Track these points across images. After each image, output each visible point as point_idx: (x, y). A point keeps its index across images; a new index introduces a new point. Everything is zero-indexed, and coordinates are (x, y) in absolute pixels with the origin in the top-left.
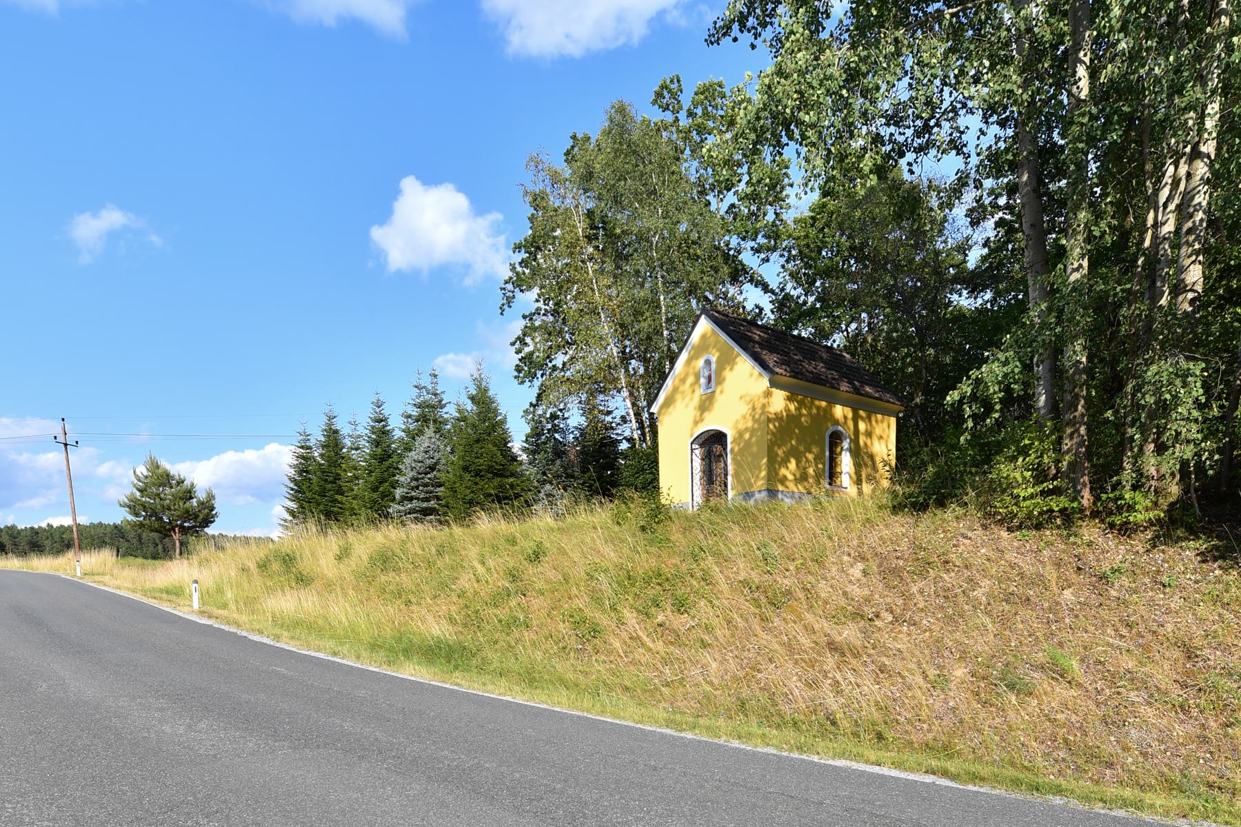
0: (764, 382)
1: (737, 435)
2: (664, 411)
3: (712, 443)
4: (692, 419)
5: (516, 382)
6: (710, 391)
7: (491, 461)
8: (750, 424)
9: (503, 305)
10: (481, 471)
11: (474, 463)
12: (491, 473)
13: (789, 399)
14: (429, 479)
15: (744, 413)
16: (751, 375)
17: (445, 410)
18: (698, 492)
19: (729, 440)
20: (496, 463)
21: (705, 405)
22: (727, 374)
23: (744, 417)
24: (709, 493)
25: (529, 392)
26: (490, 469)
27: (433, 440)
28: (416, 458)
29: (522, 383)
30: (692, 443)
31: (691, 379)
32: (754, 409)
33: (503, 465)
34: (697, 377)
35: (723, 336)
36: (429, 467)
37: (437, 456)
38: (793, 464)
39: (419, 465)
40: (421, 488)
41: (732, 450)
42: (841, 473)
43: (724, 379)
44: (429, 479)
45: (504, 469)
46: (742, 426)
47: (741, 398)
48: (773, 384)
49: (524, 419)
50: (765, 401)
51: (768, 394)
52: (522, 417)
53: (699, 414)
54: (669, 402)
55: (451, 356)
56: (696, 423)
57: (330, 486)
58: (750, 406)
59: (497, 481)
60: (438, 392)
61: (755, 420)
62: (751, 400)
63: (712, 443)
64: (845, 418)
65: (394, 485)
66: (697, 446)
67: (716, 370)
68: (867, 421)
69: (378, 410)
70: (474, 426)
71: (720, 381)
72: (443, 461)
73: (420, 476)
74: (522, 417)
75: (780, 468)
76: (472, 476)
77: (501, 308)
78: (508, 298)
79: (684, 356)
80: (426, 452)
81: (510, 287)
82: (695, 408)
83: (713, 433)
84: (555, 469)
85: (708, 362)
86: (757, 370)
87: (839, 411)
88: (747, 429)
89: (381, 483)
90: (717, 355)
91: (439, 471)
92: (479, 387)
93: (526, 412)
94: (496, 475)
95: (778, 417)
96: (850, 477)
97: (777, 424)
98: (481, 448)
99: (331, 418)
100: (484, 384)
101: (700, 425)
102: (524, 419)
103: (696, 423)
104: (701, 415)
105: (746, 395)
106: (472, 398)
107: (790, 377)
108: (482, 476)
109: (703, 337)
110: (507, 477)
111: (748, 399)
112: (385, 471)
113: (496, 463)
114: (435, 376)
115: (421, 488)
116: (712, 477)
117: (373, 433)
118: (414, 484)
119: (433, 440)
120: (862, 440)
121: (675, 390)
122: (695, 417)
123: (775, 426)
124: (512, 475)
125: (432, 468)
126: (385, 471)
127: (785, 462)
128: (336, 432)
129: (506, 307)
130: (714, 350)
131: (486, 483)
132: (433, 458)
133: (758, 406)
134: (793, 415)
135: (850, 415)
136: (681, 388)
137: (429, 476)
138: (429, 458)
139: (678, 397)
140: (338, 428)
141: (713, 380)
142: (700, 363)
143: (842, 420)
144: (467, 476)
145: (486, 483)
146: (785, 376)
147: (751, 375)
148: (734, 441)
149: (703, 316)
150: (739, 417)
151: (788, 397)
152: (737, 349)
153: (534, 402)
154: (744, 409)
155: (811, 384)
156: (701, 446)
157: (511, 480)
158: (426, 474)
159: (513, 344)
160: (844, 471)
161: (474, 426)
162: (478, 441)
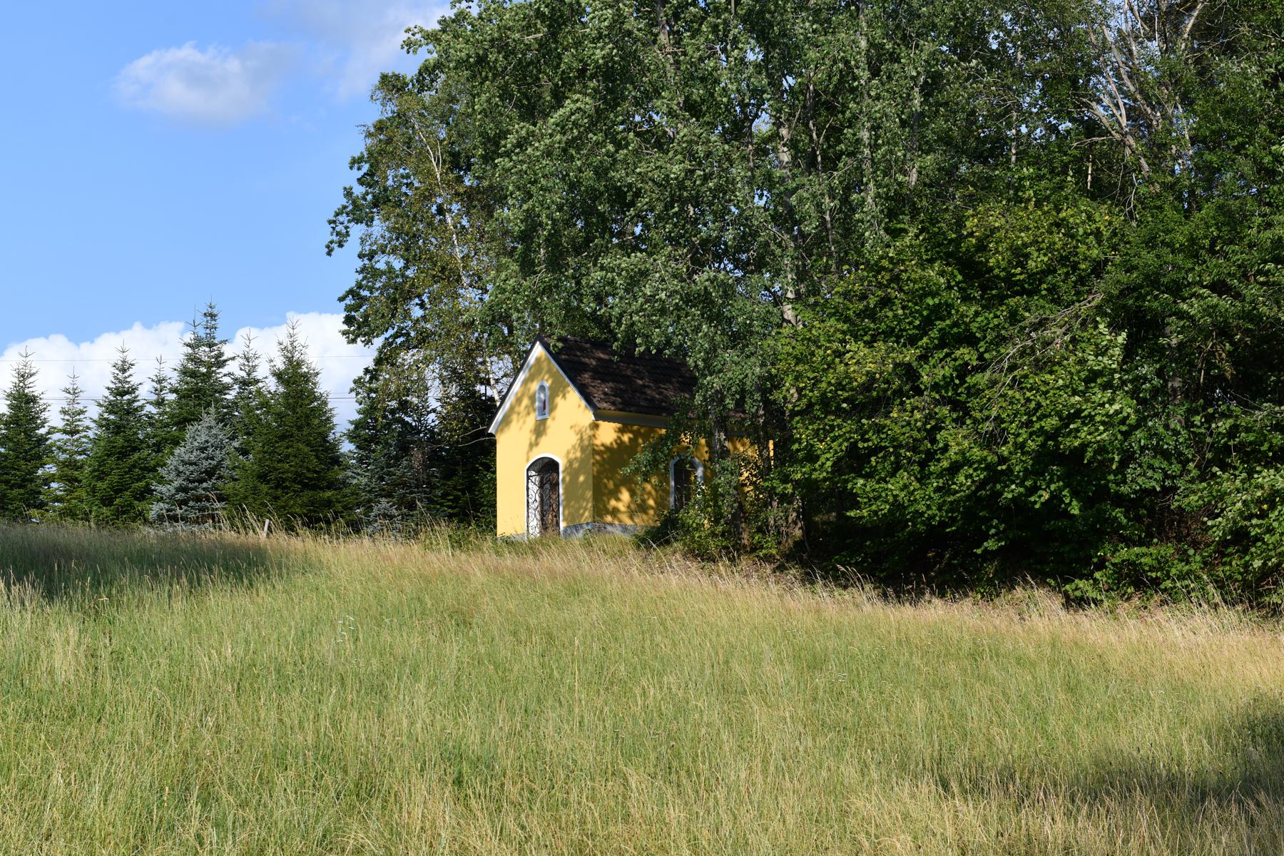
0: (589, 416)
3: (546, 469)
4: (527, 443)
5: (344, 339)
7: (301, 467)
8: (578, 454)
9: (332, 242)
10: (284, 480)
11: (276, 470)
12: (298, 483)
14: (204, 489)
17: (224, 370)
18: (535, 522)
19: (561, 468)
20: (309, 470)
21: (540, 430)
22: (559, 400)
23: (574, 447)
24: (544, 526)
25: (363, 356)
26: (298, 478)
27: (214, 431)
28: (186, 458)
29: (354, 341)
30: (528, 470)
32: (582, 439)
33: (316, 472)
35: (556, 367)
36: (206, 472)
37: (218, 454)
38: (625, 496)
39: (191, 468)
40: (191, 503)
41: (564, 479)
44: (204, 489)
45: (318, 479)
46: (572, 456)
49: (353, 394)
51: (595, 426)
52: (352, 390)
54: (506, 421)
55: (186, 53)
56: (533, 445)
57: (15, 492)
58: (579, 436)
59: (307, 495)
60: (216, 341)
63: (546, 469)
65: (145, 494)
66: (534, 473)
69: (121, 376)
70: (280, 416)
71: (553, 409)
72: (227, 462)
73: (190, 485)
74: (352, 390)
75: (609, 500)
76: (271, 488)
77: (328, 247)
78: (338, 234)
80: (203, 449)
81: (343, 218)
83: (547, 461)
84: (398, 473)
86: (583, 403)
88: (576, 458)
89: (117, 492)
90: (550, 382)
91: (220, 477)
92: (290, 360)
93: (358, 382)
94: (306, 486)
95: (608, 449)
98: (287, 448)
99: (23, 377)
100: (297, 355)
101: (535, 449)
102: (353, 394)
103: (533, 445)
104: (536, 439)
106: (279, 376)
108: (287, 487)
109: (538, 360)
110: (322, 489)
111: (577, 429)
112: (126, 473)
113: (309, 470)
114: (213, 316)
115: (191, 503)
116: (548, 509)
117: (110, 413)
118: (180, 496)
119: (214, 431)
121: (512, 409)
124: (331, 485)
125: (210, 473)
126: (126, 473)
127: (615, 494)
128: (32, 400)
129: (335, 246)
131: (291, 498)
132: (212, 459)
133: (585, 437)
134: (626, 446)
136: (517, 409)
137: (205, 485)
138: (207, 459)
139: (514, 417)
140: (36, 394)
141: (546, 408)
144: (264, 488)
145: (291, 498)
150: (570, 447)
153: (372, 366)
154: (573, 439)
156: (539, 472)
157: (328, 494)
158: (201, 481)
159: (341, 299)
161: (280, 416)
162: (283, 437)
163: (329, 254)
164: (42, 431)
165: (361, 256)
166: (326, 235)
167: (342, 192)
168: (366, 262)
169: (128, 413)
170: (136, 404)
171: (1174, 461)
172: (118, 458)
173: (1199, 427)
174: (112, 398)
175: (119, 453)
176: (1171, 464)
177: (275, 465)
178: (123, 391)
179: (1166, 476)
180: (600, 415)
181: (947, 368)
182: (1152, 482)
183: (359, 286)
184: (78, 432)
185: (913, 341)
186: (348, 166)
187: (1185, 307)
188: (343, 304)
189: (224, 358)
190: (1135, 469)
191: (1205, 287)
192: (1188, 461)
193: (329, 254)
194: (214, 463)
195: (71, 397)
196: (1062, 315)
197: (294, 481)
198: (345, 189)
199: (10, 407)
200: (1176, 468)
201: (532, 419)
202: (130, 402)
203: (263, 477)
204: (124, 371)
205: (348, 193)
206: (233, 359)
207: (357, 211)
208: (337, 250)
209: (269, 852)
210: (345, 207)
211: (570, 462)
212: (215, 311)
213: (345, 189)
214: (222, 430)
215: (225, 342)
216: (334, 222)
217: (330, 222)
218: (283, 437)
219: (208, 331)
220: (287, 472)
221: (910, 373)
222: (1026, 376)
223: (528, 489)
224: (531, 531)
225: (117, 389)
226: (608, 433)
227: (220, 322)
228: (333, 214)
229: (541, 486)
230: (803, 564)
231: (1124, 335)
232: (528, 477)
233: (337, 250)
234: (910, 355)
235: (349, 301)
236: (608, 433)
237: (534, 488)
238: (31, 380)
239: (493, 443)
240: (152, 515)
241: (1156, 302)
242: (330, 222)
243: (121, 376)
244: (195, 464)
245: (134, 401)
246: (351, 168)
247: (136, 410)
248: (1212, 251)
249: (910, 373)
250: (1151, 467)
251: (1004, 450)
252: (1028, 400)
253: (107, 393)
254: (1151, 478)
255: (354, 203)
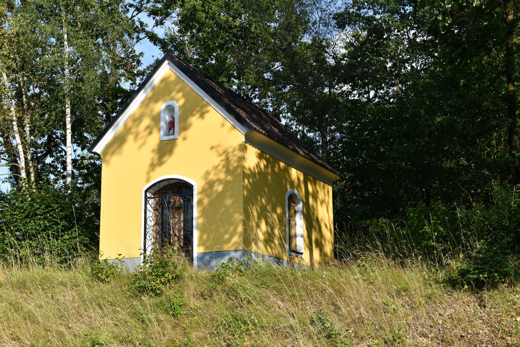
1: (207, 186)
2: (112, 149)
4: (149, 162)
6: (171, 137)
13: (260, 157)
15: (216, 164)
16: (223, 125)
22: (195, 120)
23: (216, 168)
31: (146, 122)
32: (227, 159)
34: (156, 119)
42: (296, 236)
43: (190, 125)
47: (212, 148)
48: (249, 140)
50: (240, 154)
51: (243, 148)
53: (156, 157)
56: (153, 166)
58: (223, 157)
61: (228, 171)
62: (225, 151)
64: (299, 179)
67: (180, 117)
68: (313, 184)
71: (185, 128)
79: (141, 97)
82: (153, 151)
85: (170, 109)
87: (294, 173)
95: (253, 174)
96: (304, 240)
97: (251, 181)
101: (158, 170)
103: (153, 166)
105: (218, 146)
107: (264, 134)
109: (164, 80)
111: (221, 150)
120: (311, 200)
121: (127, 131)
122: (153, 159)
123: (249, 181)
130: (180, 95)
135: (302, 178)
139: (130, 138)
142: (160, 106)
143: (296, 182)
146: (261, 133)
147: (223, 125)
148: (203, 191)
149: (166, 62)
150: (209, 167)
151: (259, 154)
152: (207, 98)
154: (217, 160)
155: (279, 144)
160: (298, 233)
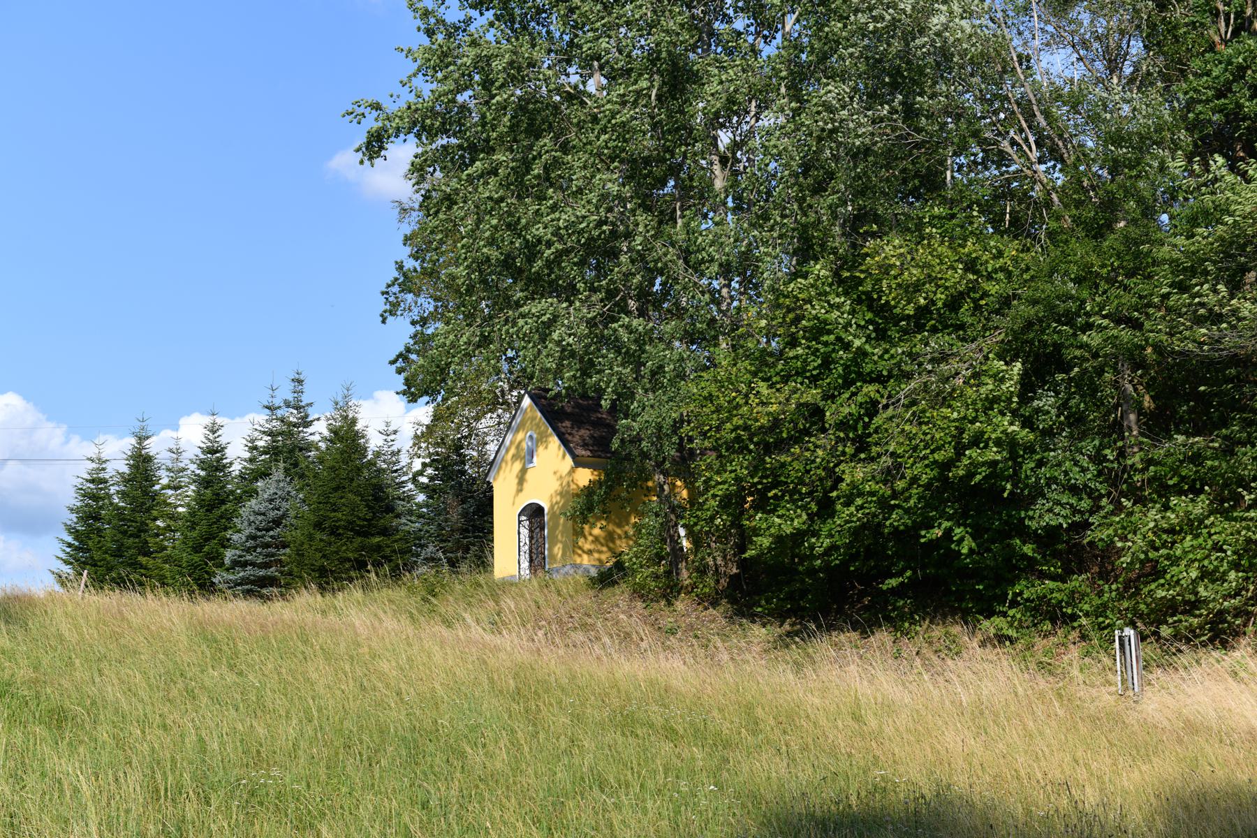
0: (569, 461)
3: (534, 513)
9: (385, 312)
10: (338, 528)
12: (351, 531)
17: (310, 430)
18: (525, 564)
19: (546, 511)
26: (350, 526)
27: (281, 484)
30: (519, 515)
36: (274, 521)
39: (260, 518)
51: (572, 471)
63: (534, 513)
69: (211, 437)
77: (382, 316)
80: (271, 501)
81: (396, 289)
89: (207, 540)
94: (358, 534)
108: (340, 534)
110: (373, 535)
111: (558, 475)
113: (359, 518)
114: (300, 382)
119: (281, 484)
125: (277, 522)
126: (215, 523)
128: (148, 459)
137: (271, 533)
157: (377, 539)
158: (267, 530)
159: (393, 362)
162: (336, 489)
163: (384, 322)
164: (157, 487)
165: (413, 323)
166: (381, 305)
167: (393, 266)
168: (418, 328)
169: (217, 469)
170: (225, 461)
171: (1084, 496)
172: (207, 511)
173: (1112, 462)
174: (202, 456)
175: (208, 505)
176: (1081, 499)
177: (328, 513)
178: (214, 450)
179: (1075, 511)
180: (579, 463)
181: (853, 406)
182: (1060, 519)
183: (408, 350)
184: (180, 487)
185: (814, 380)
186: (401, 243)
187: (1085, 338)
188: (394, 367)
189: (309, 419)
190: (1044, 504)
191: (1104, 317)
192: (1101, 496)
193: (384, 322)
194: (280, 513)
195: (175, 456)
196: (968, 349)
197: (345, 528)
198: (396, 263)
199: (131, 466)
200: (1085, 504)
201: (518, 466)
202: (219, 460)
203: (318, 526)
204: (214, 432)
205: (400, 267)
206: (318, 419)
207: (406, 282)
208: (390, 319)
209: (848, 836)
210: (396, 279)
211: (552, 507)
212: (302, 377)
213: (396, 263)
214: (289, 483)
215: (310, 405)
216: (387, 293)
217: (383, 293)
218: (336, 489)
219: (296, 395)
220: (339, 520)
221: (816, 413)
222: (924, 411)
223: (519, 533)
224: (522, 573)
225: (207, 447)
226: (585, 477)
227: (306, 387)
228: (385, 285)
229: (531, 531)
230: (733, 601)
231: (1019, 365)
232: (520, 522)
233: (390, 319)
234: (812, 395)
235: (400, 364)
236: (585, 477)
237: (525, 532)
238: (146, 443)
239: (490, 489)
240: (227, 561)
241: (1057, 332)
242: (383, 293)
243: (211, 437)
244: (264, 514)
245: (222, 459)
246: (405, 244)
247: (224, 466)
248: (1111, 281)
249: (816, 413)
250: (1058, 503)
251: (900, 485)
252: (925, 434)
253: (199, 452)
254: (1059, 514)
255: (405, 275)
